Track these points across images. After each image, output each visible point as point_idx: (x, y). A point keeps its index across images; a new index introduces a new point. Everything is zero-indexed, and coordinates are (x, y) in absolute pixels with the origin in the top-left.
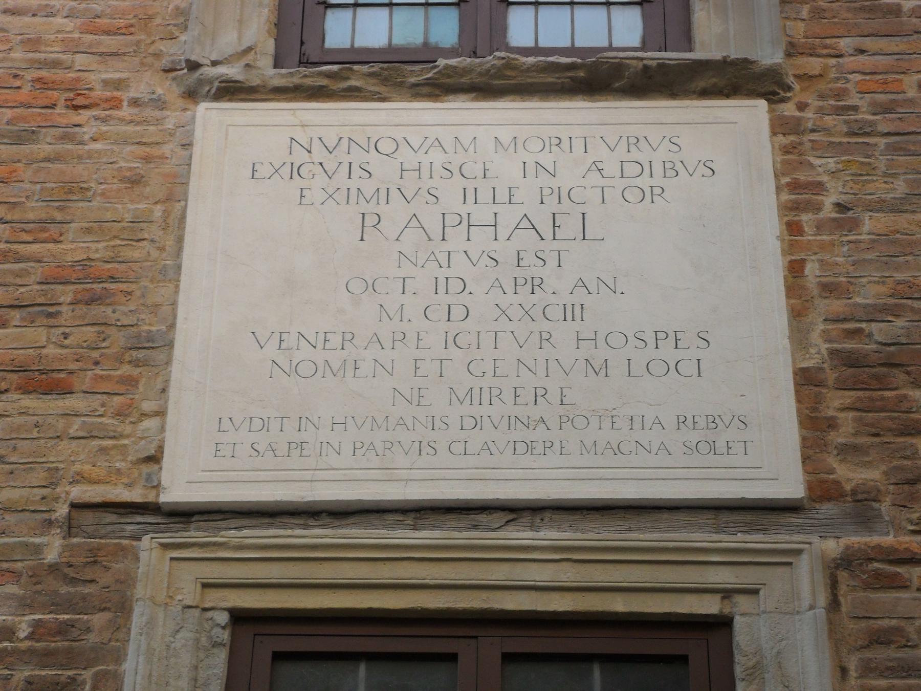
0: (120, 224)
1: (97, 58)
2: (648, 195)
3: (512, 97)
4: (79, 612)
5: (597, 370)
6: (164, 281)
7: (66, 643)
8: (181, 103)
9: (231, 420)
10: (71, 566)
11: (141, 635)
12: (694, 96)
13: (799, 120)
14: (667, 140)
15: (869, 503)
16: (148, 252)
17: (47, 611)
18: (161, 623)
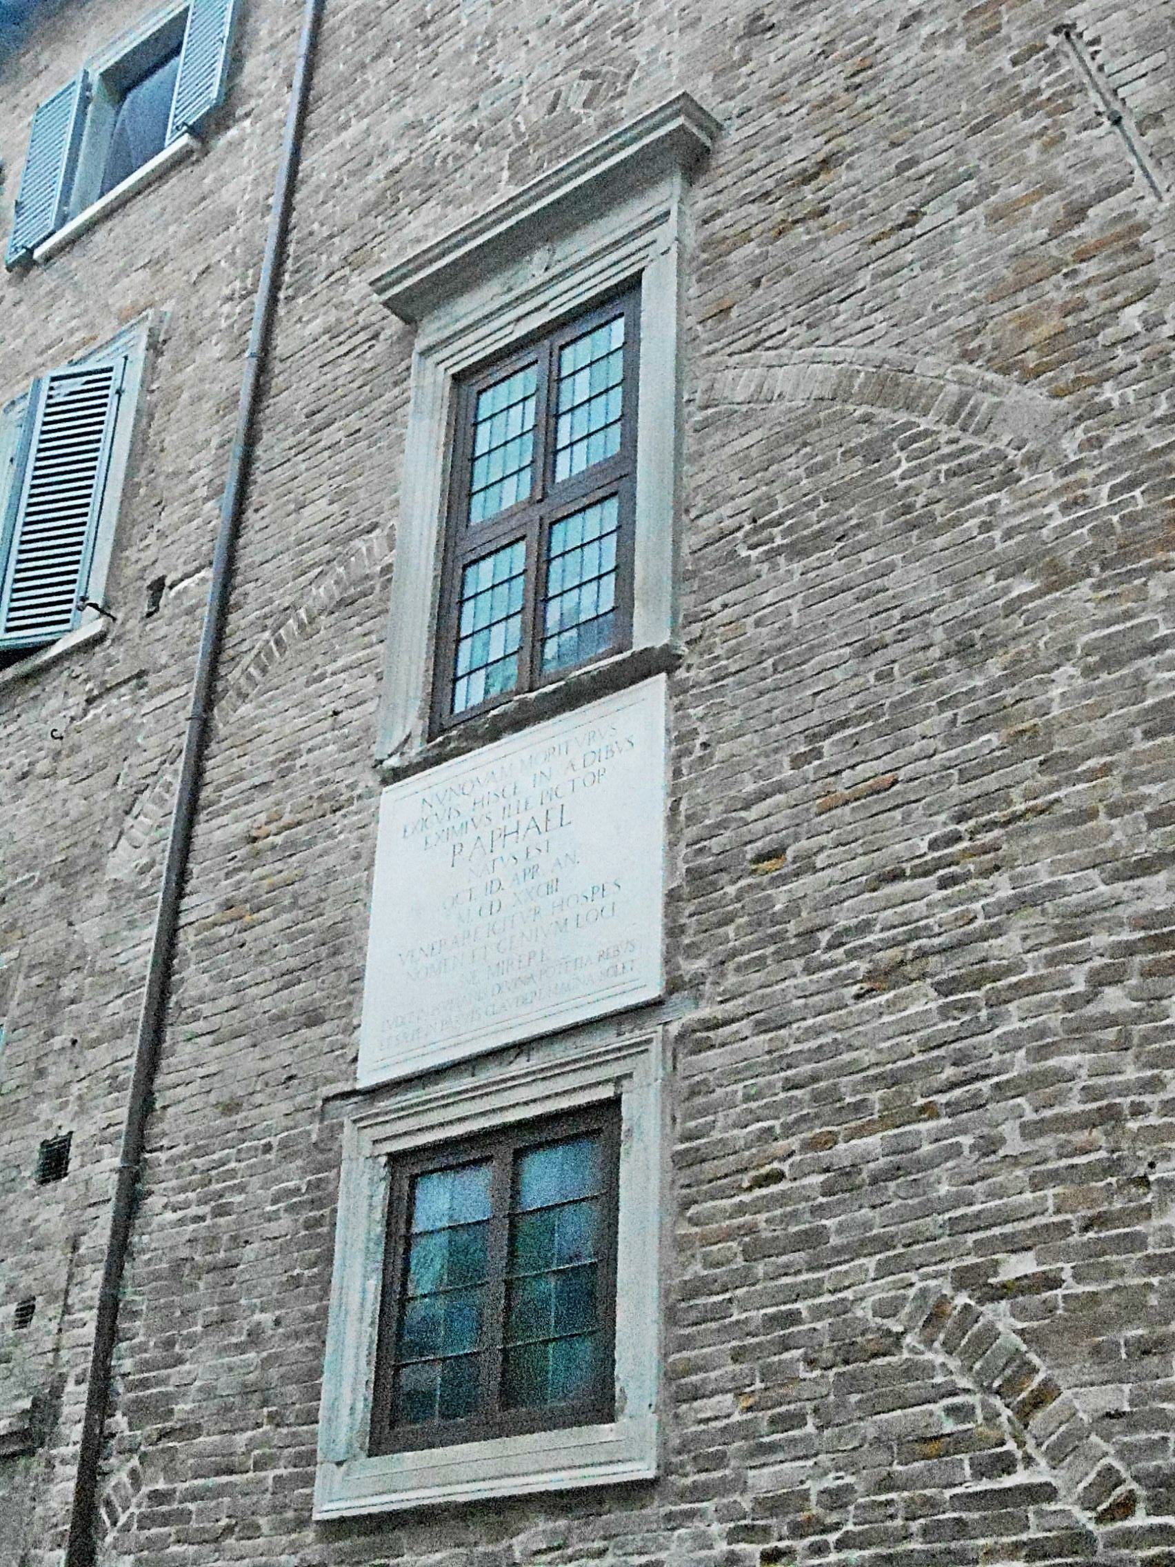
2: (596, 777)
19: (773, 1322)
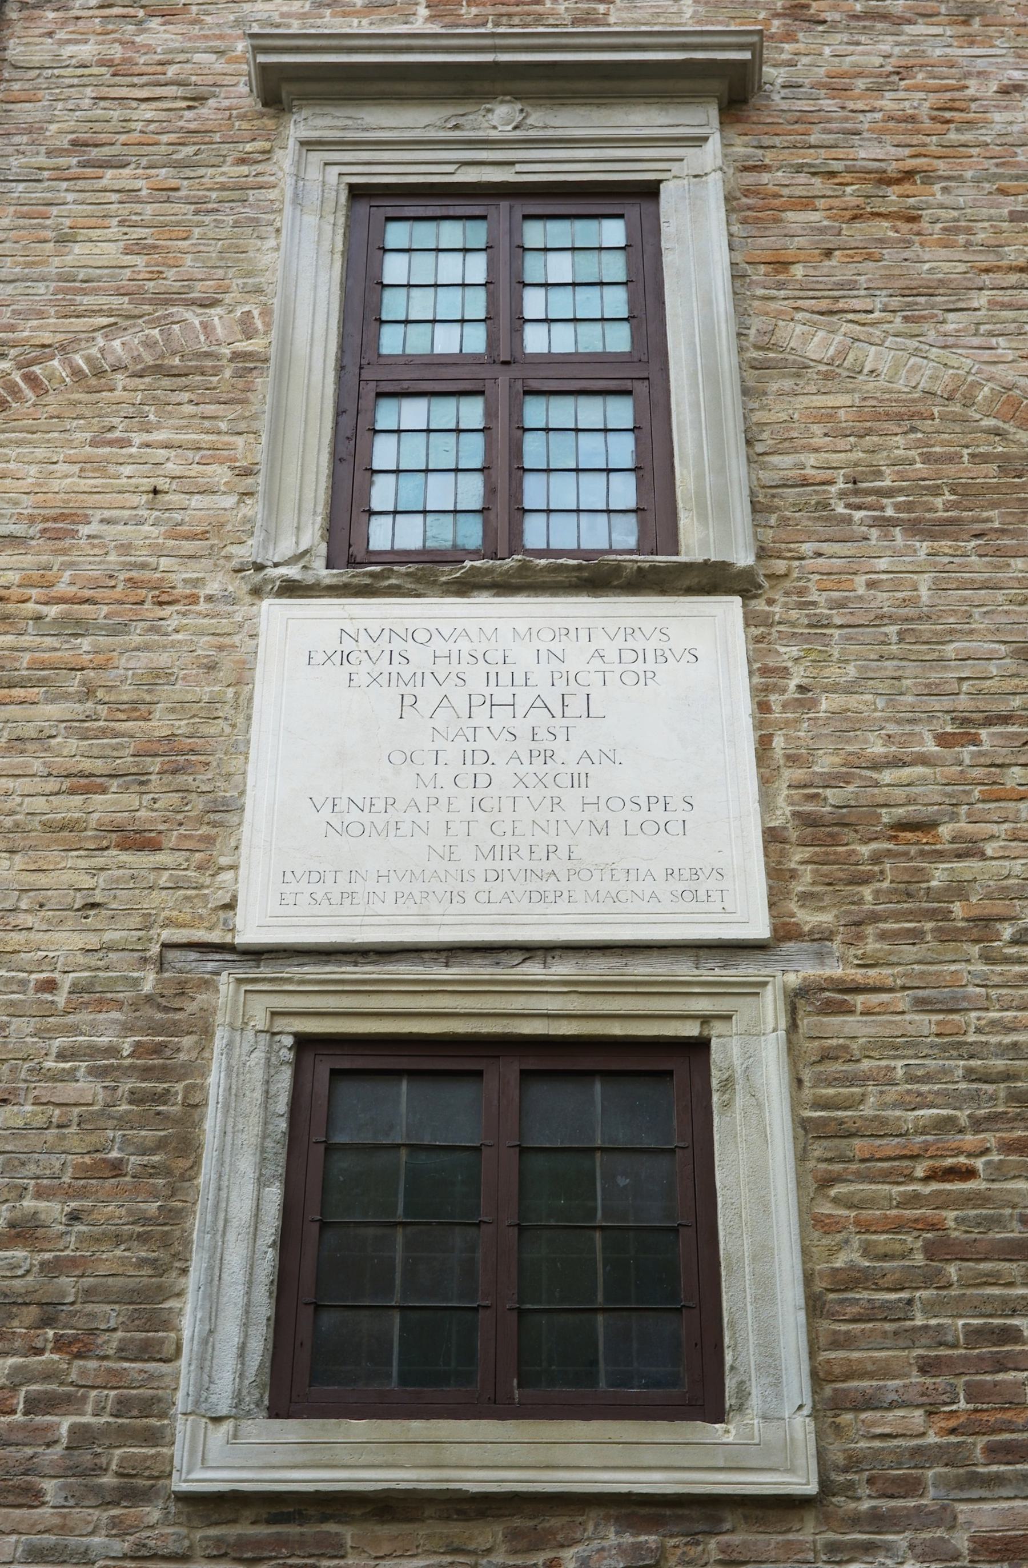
19: (975, 1335)
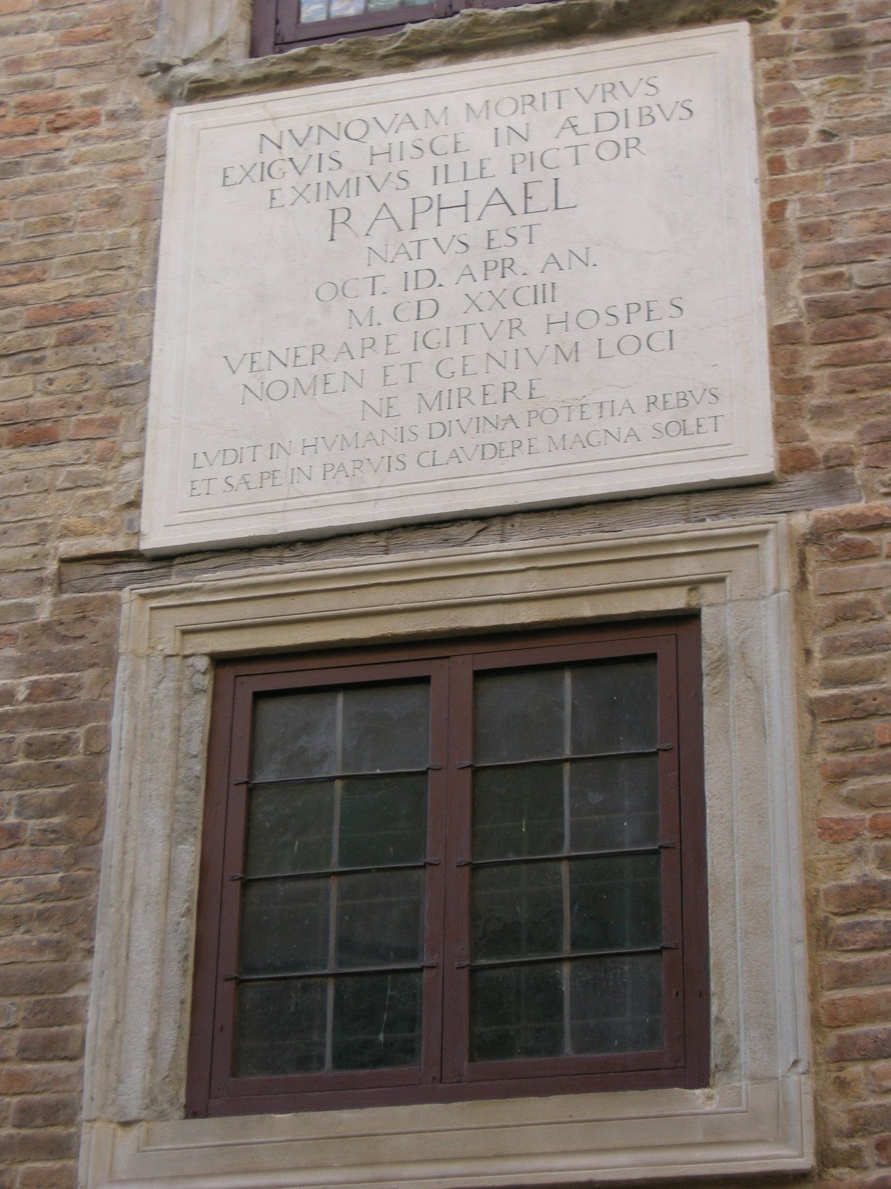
0: (99, 253)
1: (76, 71)
2: (623, 149)
3: (484, 55)
4: (71, 670)
5: (567, 355)
6: (141, 311)
7: (60, 703)
8: (156, 109)
9: (206, 455)
10: (62, 624)
11: (124, 690)
12: (673, 27)
13: (783, 39)
14: (644, 82)
15: (842, 468)
16: (126, 281)
17: (42, 672)
18: (144, 676)
